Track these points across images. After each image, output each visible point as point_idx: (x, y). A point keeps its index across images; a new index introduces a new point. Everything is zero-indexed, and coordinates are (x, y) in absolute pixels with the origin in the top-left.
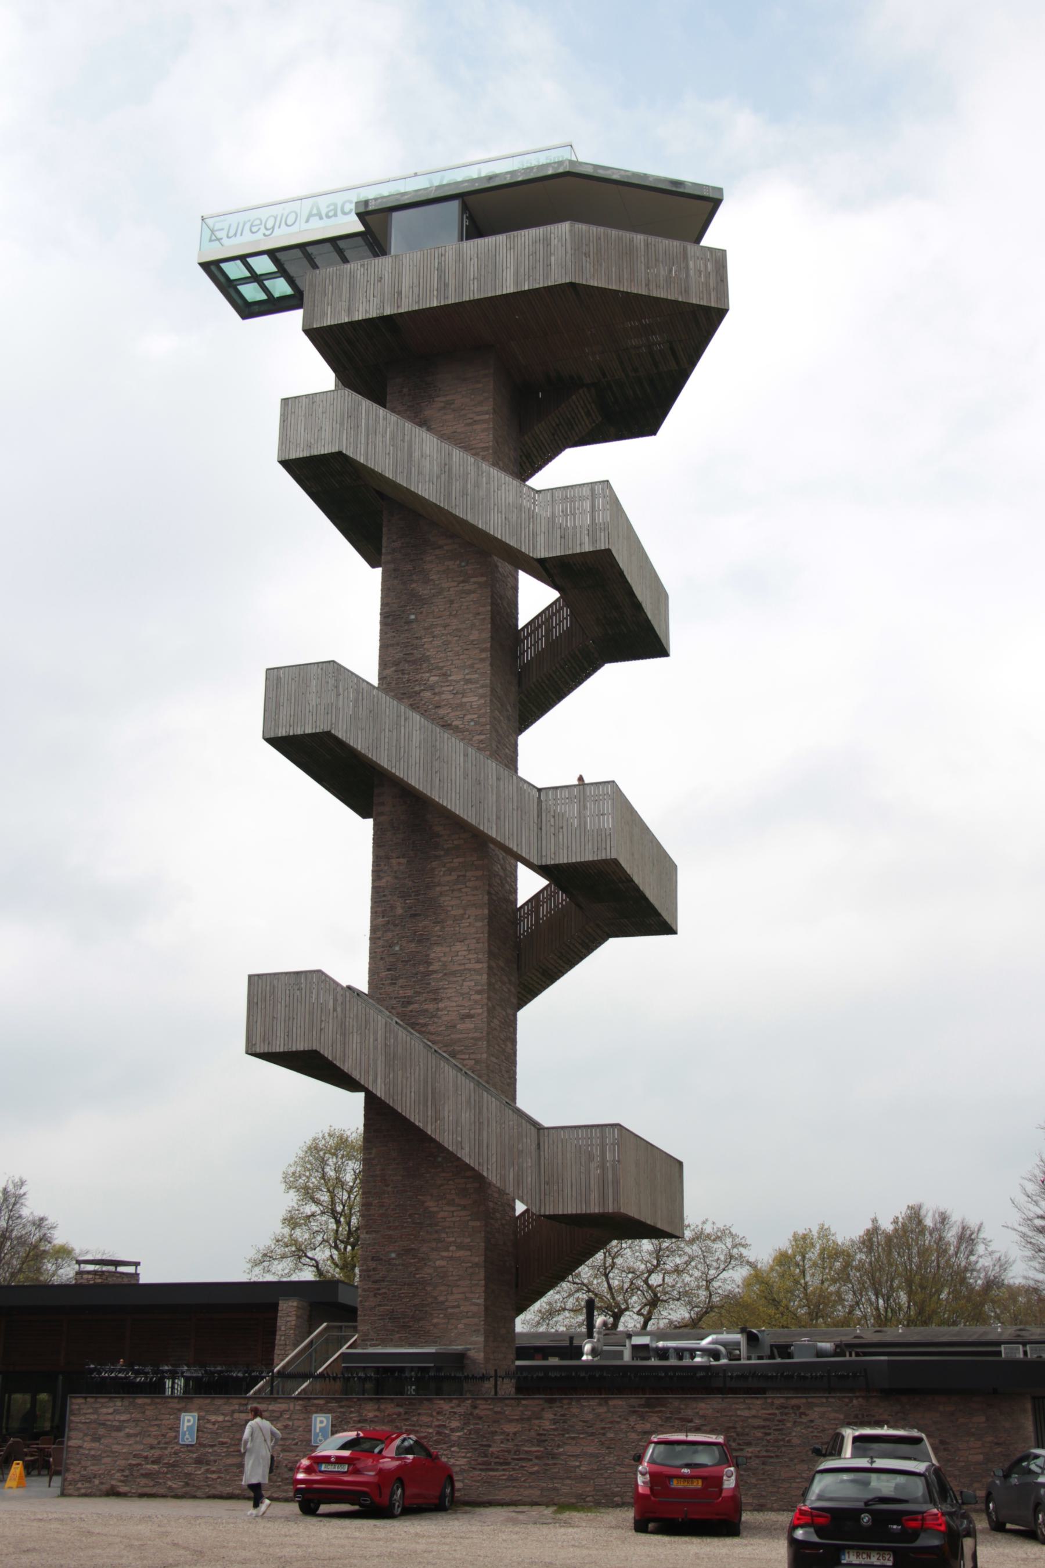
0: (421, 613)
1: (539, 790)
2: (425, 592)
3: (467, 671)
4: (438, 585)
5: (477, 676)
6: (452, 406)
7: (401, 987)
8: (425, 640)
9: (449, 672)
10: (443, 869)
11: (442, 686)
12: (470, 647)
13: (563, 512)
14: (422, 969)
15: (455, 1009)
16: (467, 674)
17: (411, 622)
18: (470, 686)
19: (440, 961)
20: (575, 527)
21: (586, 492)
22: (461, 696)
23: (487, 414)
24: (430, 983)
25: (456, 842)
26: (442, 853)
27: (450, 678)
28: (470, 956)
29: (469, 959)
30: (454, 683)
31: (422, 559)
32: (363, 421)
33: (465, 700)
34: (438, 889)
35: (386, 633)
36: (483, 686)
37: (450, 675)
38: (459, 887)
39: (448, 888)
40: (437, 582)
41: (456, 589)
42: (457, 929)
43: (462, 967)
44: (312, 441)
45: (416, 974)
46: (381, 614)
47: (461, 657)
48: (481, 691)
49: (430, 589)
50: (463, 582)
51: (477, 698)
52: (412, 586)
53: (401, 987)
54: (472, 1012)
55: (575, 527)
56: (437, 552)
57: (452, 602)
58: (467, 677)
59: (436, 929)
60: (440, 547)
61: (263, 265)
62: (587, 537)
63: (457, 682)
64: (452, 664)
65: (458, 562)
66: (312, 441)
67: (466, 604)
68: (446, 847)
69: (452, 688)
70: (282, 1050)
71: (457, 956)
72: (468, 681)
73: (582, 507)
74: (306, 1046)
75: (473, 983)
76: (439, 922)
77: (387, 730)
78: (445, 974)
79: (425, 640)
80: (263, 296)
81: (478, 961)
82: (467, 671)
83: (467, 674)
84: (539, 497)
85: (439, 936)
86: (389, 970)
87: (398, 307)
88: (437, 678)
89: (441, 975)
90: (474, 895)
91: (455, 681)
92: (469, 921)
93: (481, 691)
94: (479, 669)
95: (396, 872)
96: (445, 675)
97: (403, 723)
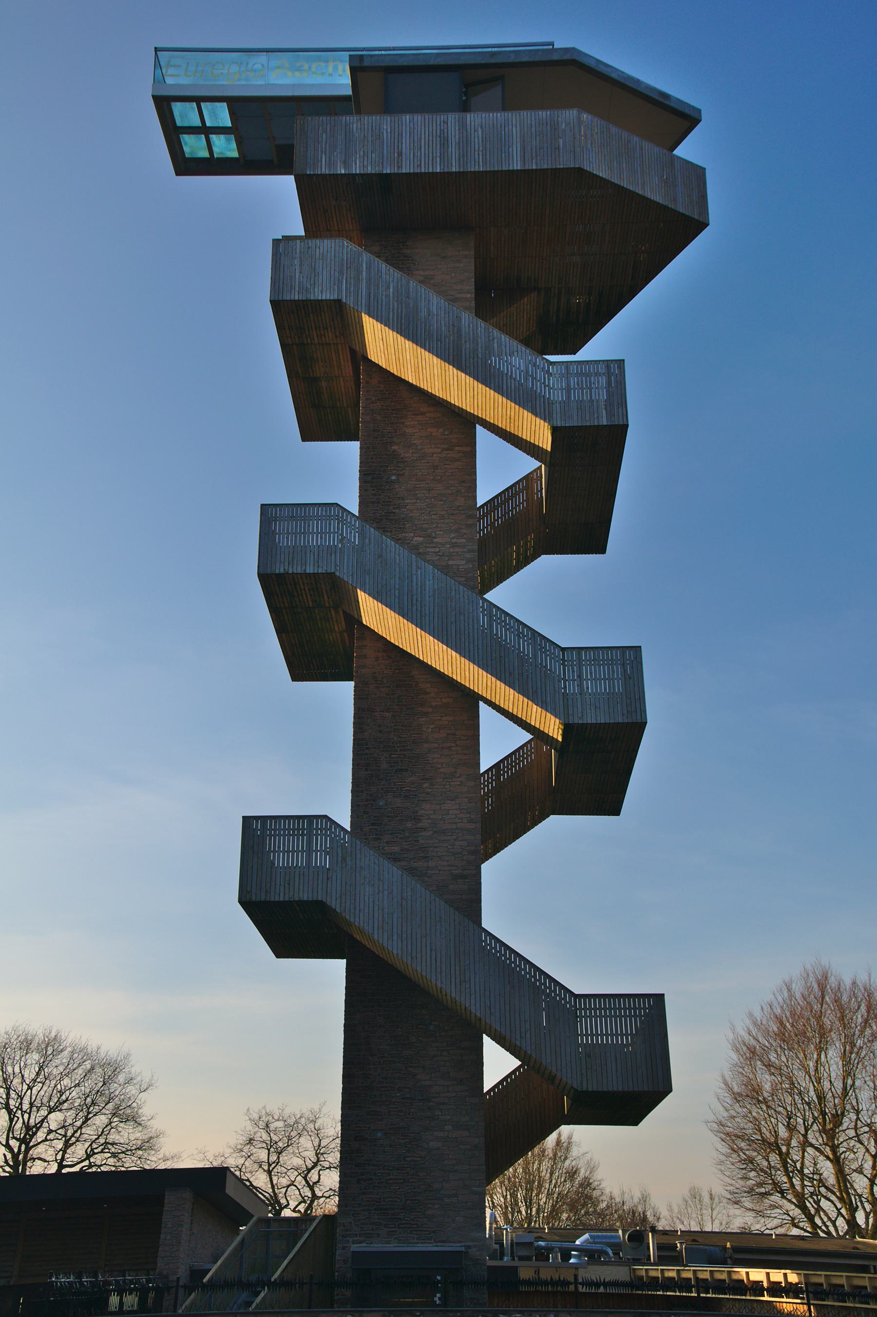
0: (403, 475)
1: (563, 649)
2: (407, 455)
3: (452, 535)
4: (421, 449)
5: (464, 540)
6: (432, 281)
7: (387, 842)
8: (408, 501)
9: (434, 535)
10: (431, 726)
11: (427, 547)
12: (455, 512)
13: (578, 384)
14: (409, 825)
15: (447, 868)
16: (453, 538)
17: (393, 482)
18: (457, 550)
19: (429, 819)
20: (591, 401)
21: (602, 369)
22: (447, 558)
23: (468, 293)
24: (418, 841)
25: (444, 701)
26: (430, 710)
27: (435, 540)
28: (461, 815)
29: (461, 819)
30: (439, 546)
31: (403, 423)
32: (364, 273)
33: (450, 563)
34: (425, 745)
35: (366, 490)
36: (470, 551)
37: (435, 538)
38: (448, 745)
39: (436, 745)
40: (419, 447)
41: (440, 455)
42: (447, 787)
43: (454, 826)
44: (308, 286)
45: (403, 830)
46: (360, 471)
47: (446, 521)
48: (468, 556)
49: (413, 453)
50: (446, 450)
51: (464, 562)
52: (393, 448)
53: (387, 842)
54: (465, 872)
55: (591, 401)
56: (420, 418)
57: (436, 467)
58: (454, 541)
59: (425, 786)
60: (423, 414)
61: (221, 116)
62: (604, 411)
63: (443, 545)
64: (437, 527)
65: (441, 430)
66: (308, 286)
67: (450, 471)
68: (434, 704)
69: (437, 550)
70: (282, 899)
71: (448, 814)
72: (454, 545)
73: (598, 382)
74: (310, 895)
75: (465, 843)
76: (428, 779)
77: (397, 578)
78: (436, 832)
79: (408, 501)
80: (205, 154)
81: (470, 821)
82: (452, 535)
83: (453, 538)
84: (553, 368)
85: (428, 793)
86: (373, 824)
87: (398, 167)
88: (421, 539)
89: (430, 833)
90: (465, 754)
91: (440, 543)
92: (459, 779)
93: (468, 556)
94: (465, 534)
95: (379, 726)
96: (429, 536)
97: (414, 572)
